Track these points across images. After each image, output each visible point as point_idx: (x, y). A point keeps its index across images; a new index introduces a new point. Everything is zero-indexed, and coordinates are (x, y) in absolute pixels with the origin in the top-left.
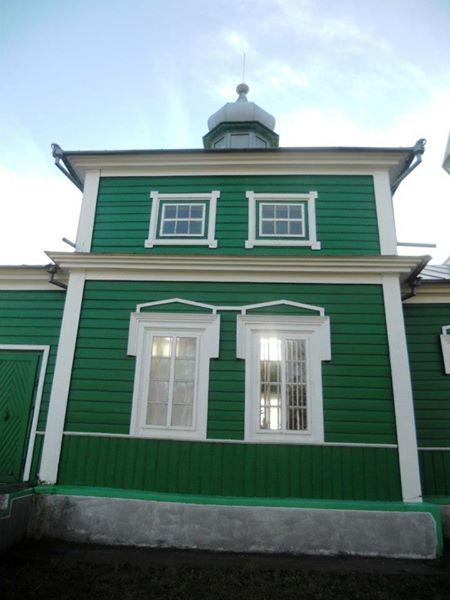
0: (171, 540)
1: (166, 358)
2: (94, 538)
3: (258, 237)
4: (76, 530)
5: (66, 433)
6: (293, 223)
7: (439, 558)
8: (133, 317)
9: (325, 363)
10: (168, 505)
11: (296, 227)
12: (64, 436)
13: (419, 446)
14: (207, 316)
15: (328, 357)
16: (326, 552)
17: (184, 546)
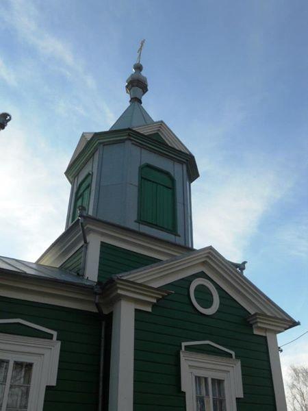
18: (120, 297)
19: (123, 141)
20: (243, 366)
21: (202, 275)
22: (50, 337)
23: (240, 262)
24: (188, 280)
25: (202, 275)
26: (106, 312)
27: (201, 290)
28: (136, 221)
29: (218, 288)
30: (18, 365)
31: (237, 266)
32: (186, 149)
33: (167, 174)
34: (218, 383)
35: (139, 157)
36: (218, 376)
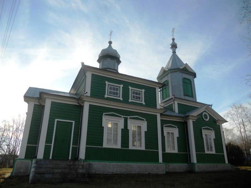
0: (115, 172)
1: (110, 128)
2: (97, 173)
3: (108, 95)
4: (92, 171)
5: (46, 144)
6: (111, 90)
7: (7, 178)
8: (103, 116)
9: (145, 132)
10: (114, 163)
11: (117, 94)
12: (45, 145)
13: (86, 145)
14: (120, 118)
15: (146, 131)
16: (146, 173)
17: (118, 173)
18: (189, 119)
19: (177, 71)
20: (147, 123)
21: (205, 111)
22: (176, 127)
23: (211, 104)
24: (202, 113)
25: (205, 111)
26: (186, 121)
27: (205, 115)
28: (83, 64)
29: (209, 114)
30: (171, 133)
31: (209, 105)
32: (193, 71)
33: (189, 80)
34: (173, 133)
35: (180, 76)
36: (172, 132)
